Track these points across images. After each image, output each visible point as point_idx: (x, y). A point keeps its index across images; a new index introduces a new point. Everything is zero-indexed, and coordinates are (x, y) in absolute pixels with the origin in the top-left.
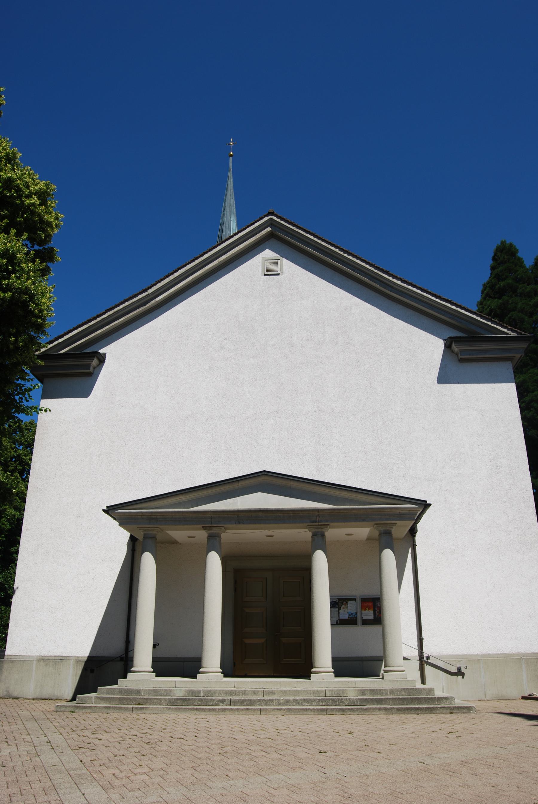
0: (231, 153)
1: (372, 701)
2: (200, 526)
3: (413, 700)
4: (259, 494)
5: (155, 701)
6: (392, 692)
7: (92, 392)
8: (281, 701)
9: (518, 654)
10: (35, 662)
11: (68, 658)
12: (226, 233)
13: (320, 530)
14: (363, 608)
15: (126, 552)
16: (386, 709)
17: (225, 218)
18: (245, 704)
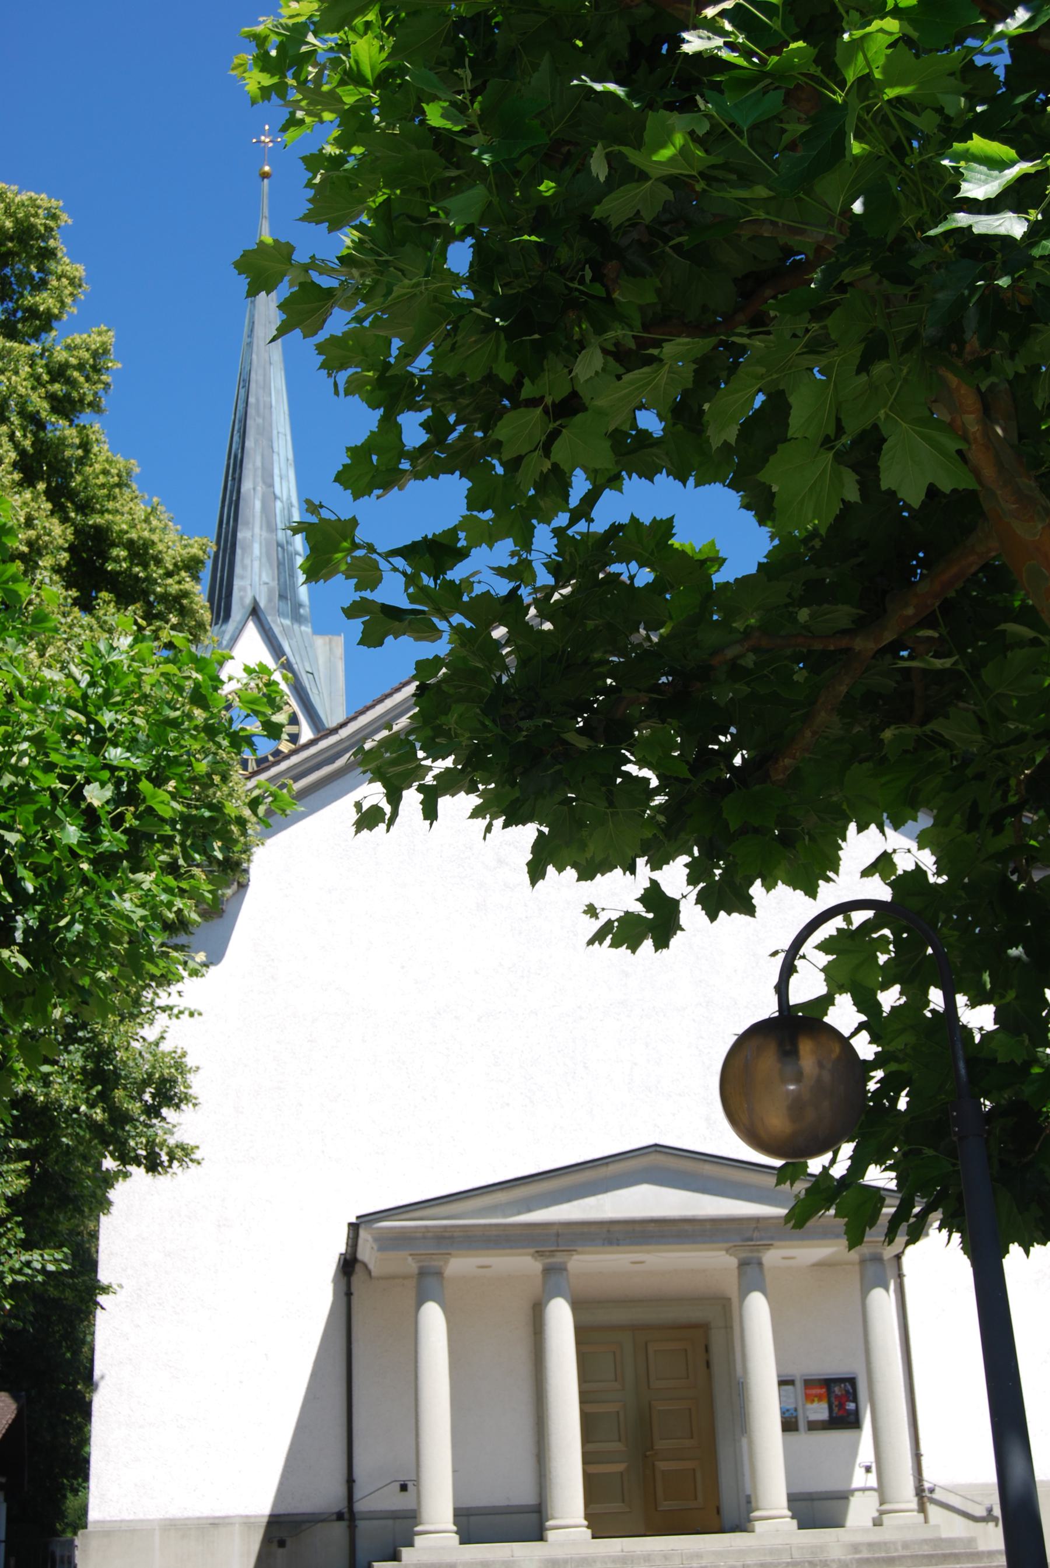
2: (532, 1250)
6: (906, 1545)
12: (257, 400)
14: (809, 1398)
17: (254, 356)
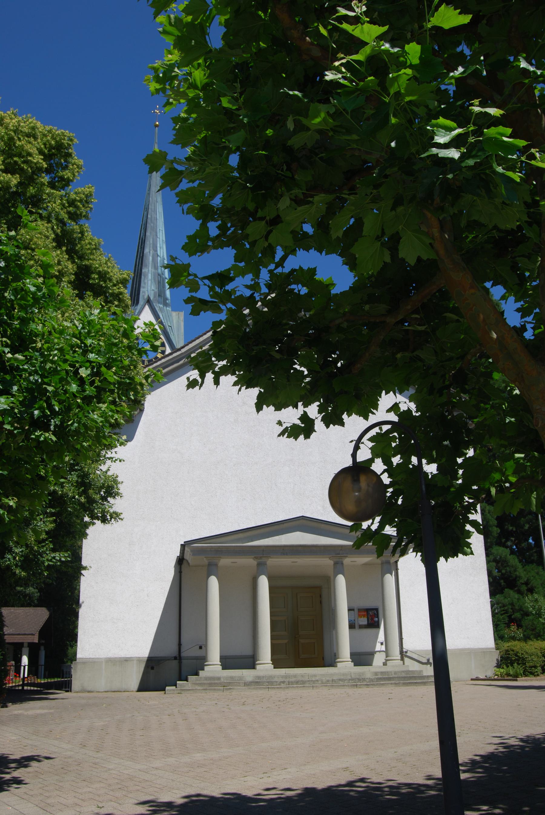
0: (157, 123)
1: (385, 679)
2: (253, 557)
3: (411, 678)
4: (298, 533)
5: (236, 684)
6: (395, 673)
7: (135, 437)
8: (324, 681)
9: (469, 649)
10: (104, 663)
11: (131, 659)
12: (151, 216)
13: (341, 560)
14: (360, 616)
15: (173, 574)
16: (395, 684)
18: (299, 683)
